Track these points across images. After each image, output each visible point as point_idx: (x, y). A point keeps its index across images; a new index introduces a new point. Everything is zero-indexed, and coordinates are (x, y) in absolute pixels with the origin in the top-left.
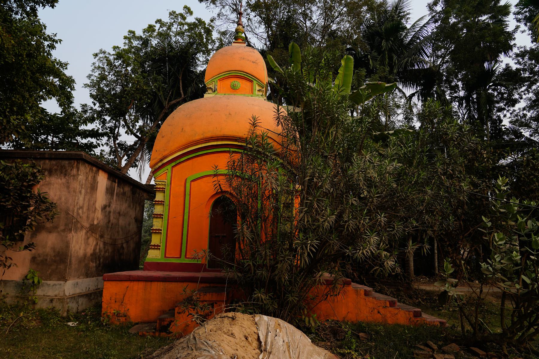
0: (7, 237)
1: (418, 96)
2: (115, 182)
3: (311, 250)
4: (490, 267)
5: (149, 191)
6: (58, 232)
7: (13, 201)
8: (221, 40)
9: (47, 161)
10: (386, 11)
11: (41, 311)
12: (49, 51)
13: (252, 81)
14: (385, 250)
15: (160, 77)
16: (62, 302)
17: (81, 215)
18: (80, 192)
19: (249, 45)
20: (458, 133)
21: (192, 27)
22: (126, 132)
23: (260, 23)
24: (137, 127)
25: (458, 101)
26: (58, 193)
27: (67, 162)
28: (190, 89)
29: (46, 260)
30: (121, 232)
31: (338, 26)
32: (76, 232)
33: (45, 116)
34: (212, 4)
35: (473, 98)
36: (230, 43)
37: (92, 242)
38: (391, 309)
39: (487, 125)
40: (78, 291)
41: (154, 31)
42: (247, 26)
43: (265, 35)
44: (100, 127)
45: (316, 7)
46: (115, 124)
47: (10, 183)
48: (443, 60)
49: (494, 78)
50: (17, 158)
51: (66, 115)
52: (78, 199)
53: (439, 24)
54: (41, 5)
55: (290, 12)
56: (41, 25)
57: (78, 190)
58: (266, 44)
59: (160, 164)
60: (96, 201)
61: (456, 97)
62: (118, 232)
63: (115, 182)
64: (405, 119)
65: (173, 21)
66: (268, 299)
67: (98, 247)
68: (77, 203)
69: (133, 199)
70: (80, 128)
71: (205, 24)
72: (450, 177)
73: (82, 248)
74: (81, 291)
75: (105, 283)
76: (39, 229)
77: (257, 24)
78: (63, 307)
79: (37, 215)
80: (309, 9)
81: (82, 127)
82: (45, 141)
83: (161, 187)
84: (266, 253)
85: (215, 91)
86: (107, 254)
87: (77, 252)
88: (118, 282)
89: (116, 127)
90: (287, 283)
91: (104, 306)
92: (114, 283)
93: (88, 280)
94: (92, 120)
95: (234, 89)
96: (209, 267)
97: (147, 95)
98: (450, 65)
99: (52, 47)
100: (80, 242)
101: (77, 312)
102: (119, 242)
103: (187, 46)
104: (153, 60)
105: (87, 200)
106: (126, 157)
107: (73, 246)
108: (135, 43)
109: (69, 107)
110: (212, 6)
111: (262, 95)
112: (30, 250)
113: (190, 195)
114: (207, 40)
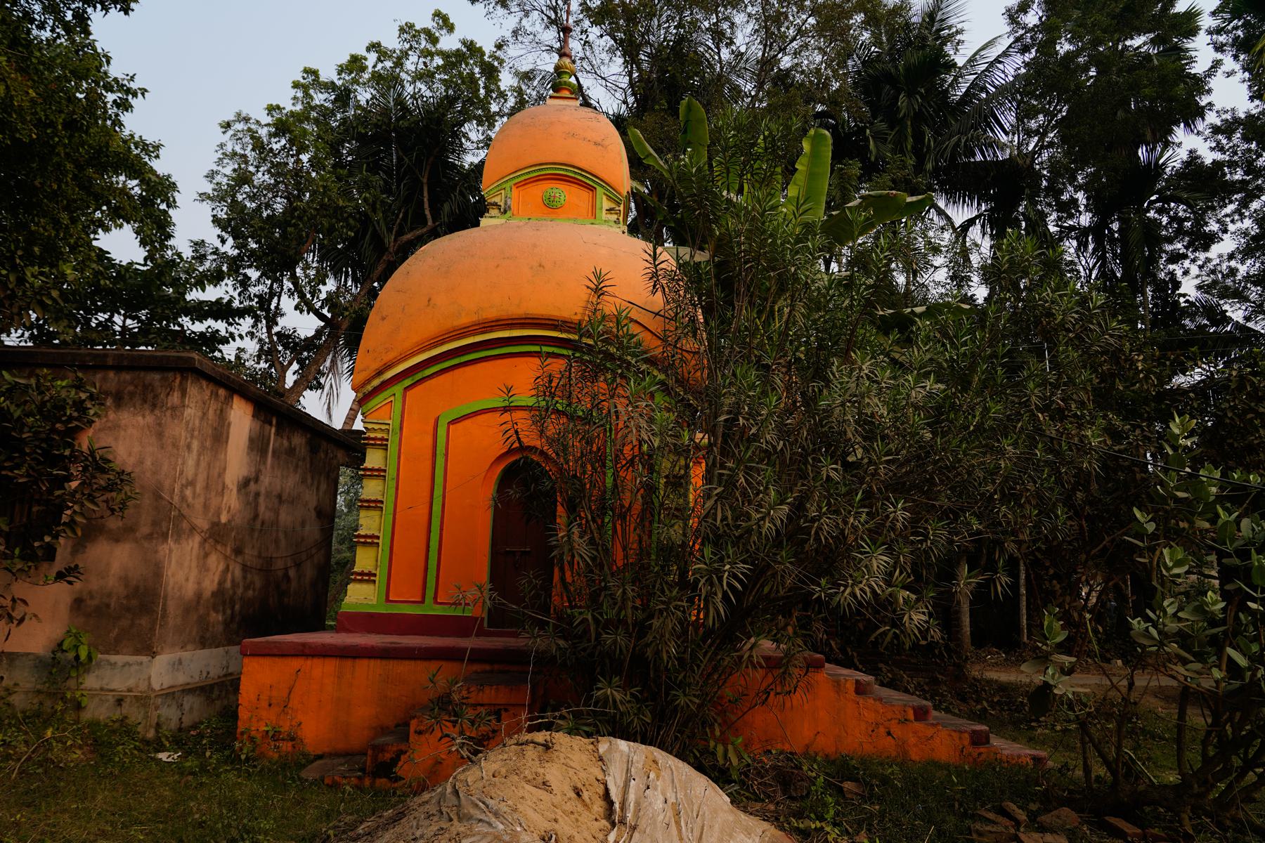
0: (17, 551)
1: (983, 226)
2: (271, 424)
4: (1152, 630)
5: (349, 446)
6: (136, 541)
8: (520, 92)
9: (111, 374)
10: (907, 25)
12: (117, 115)
13: (592, 189)
14: (905, 588)
17: (190, 500)
18: (189, 447)
19: (586, 104)
20: (1077, 312)
21: (453, 60)
22: (296, 308)
23: (611, 51)
24: (323, 296)
25: (1077, 238)
26: (137, 449)
27: (157, 376)
28: (446, 207)
29: (108, 606)
30: (283, 543)
31: (796, 61)
32: (177, 541)
33: (107, 268)
34: (499, 7)
35: (1110, 230)
36: (541, 98)
37: (215, 563)
38: (918, 725)
39: (1144, 294)
40: (181, 679)
41: (363, 69)
42: (582, 59)
43: (624, 81)
44: (236, 294)
45: (743, 15)
46: (271, 287)
47: (24, 425)
51: (156, 266)
52: (183, 464)
53: (1032, 56)
55: (683, 27)
57: (182, 443)
58: (625, 102)
59: (376, 382)
60: (225, 469)
61: (1072, 228)
62: (277, 541)
64: (952, 278)
65: (407, 46)
68: (182, 473)
69: (312, 463)
70: (188, 297)
71: (483, 54)
73: (192, 579)
74: (189, 680)
75: (246, 660)
76: (92, 532)
77: (605, 56)
78: (146, 717)
79: (88, 499)
80: (727, 19)
81: (194, 295)
82: (106, 326)
83: (379, 436)
84: (624, 593)
85: (505, 212)
86: (251, 592)
87: (180, 588)
88: (276, 659)
89: (272, 294)
91: (243, 714)
93: (206, 652)
95: (550, 206)
97: (346, 220)
98: (1058, 152)
99: (124, 106)
100: (186, 564)
101: (180, 730)
102: (279, 564)
103: (440, 104)
104: (361, 138)
105: (203, 464)
106: (295, 366)
108: (319, 98)
109: (164, 247)
111: (617, 222)
112: (70, 583)
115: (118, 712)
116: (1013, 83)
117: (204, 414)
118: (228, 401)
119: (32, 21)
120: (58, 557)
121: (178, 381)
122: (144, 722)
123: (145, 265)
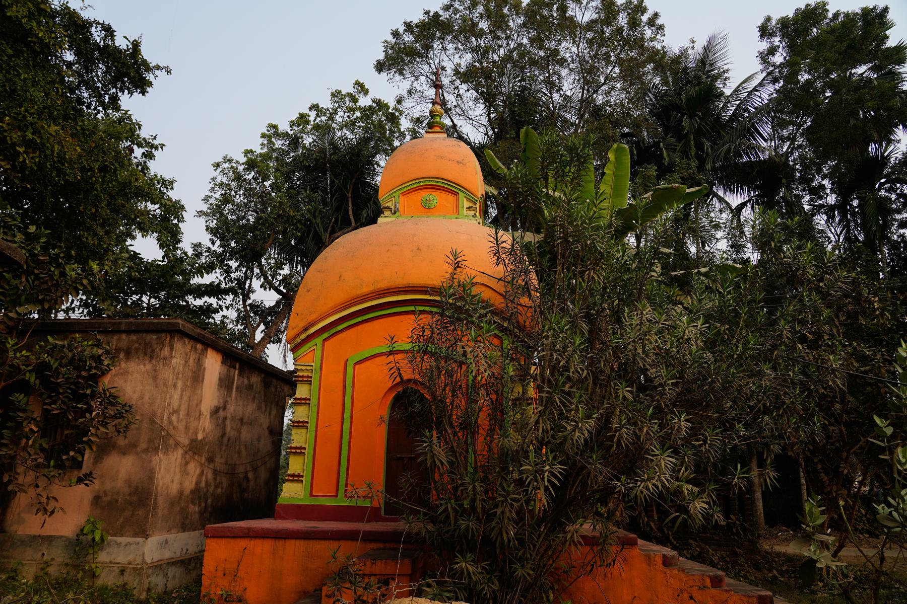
0: (52, 463)
1: (753, 207)
2: (235, 368)
3: (549, 481)
4: (895, 514)
5: (289, 380)
6: (137, 453)
7: (63, 402)
9: (124, 336)
10: (685, 69)
11: (105, 588)
12: (145, 162)
13: (456, 194)
14: (688, 482)
15: (316, 195)
16: (138, 574)
17: (175, 423)
18: (175, 386)
20: (814, 265)
21: (367, 113)
22: (261, 287)
23: (476, 100)
24: (280, 278)
25: (826, 213)
26: (139, 388)
27: (154, 337)
28: (364, 213)
29: (117, 501)
30: (244, 453)
31: (606, 99)
32: (166, 453)
33: (138, 265)
34: (397, 75)
35: (851, 206)
37: (194, 469)
38: (714, 591)
39: (882, 252)
40: (167, 555)
41: (308, 123)
42: (455, 107)
43: (484, 120)
44: (222, 279)
45: (567, 70)
46: (246, 273)
47: (59, 373)
48: (792, 143)
49: (887, 171)
50: (75, 332)
51: (170, 261)
52: (171, 398)
53: (781, 85)
54: (126, 91)
55: (525, 81)
56: (133, 124)
57: (170, 383)
59: (303, 336)
60: (201, 401)
61: (821, 206)
62: (239, 452)
63: (235, 368)
64: (732, 246)
66: (480, 573)
67: (204, 478)
68: (169, 404)
69: (265, 396)
70: (192, 282)
71: (388, 108)
72: (815, 345)
73: (176, 480)
74: (173, 555)
75: (208, 541)
76: (105, 448)
77: (471, 104)
78: (140, 583)
79: (102, 425)
81: (196, 280)
82: (137, 304)
83: (306, 374)
84: (474, 488)
85: (395, 213)
86: (219, 490)
87: (167, 488)
88: (230, 540)
89: (246, 277)
90: (514, 544)
91: (205, 581)
92: (222, 542)
93: (186, 534)
94: (210, 268)
95: (427, 207)
96: (385, 514)
97: (294, 225)
98: (809, 152)
99: (149, 156)
100: (172, 470)
101: (165, 593)
102: (241, 469)
104: (307, 169)
105: (185, 398)
106: (262, 327)
107: (159, 477)
108: (278, 143)
109: (176, 249)
110: (398, 77)
111: (475, 216)
112: (87, 485)
113: (353, 387)
114: (392, 132)
115: (121, 579)
116: (767, 104)
117: (186, 362)
118: (204, 352)
119: (83, 103)
120: (84, 466)
121: (168, 339)
122: (138, 588)
123: (163, 261)
